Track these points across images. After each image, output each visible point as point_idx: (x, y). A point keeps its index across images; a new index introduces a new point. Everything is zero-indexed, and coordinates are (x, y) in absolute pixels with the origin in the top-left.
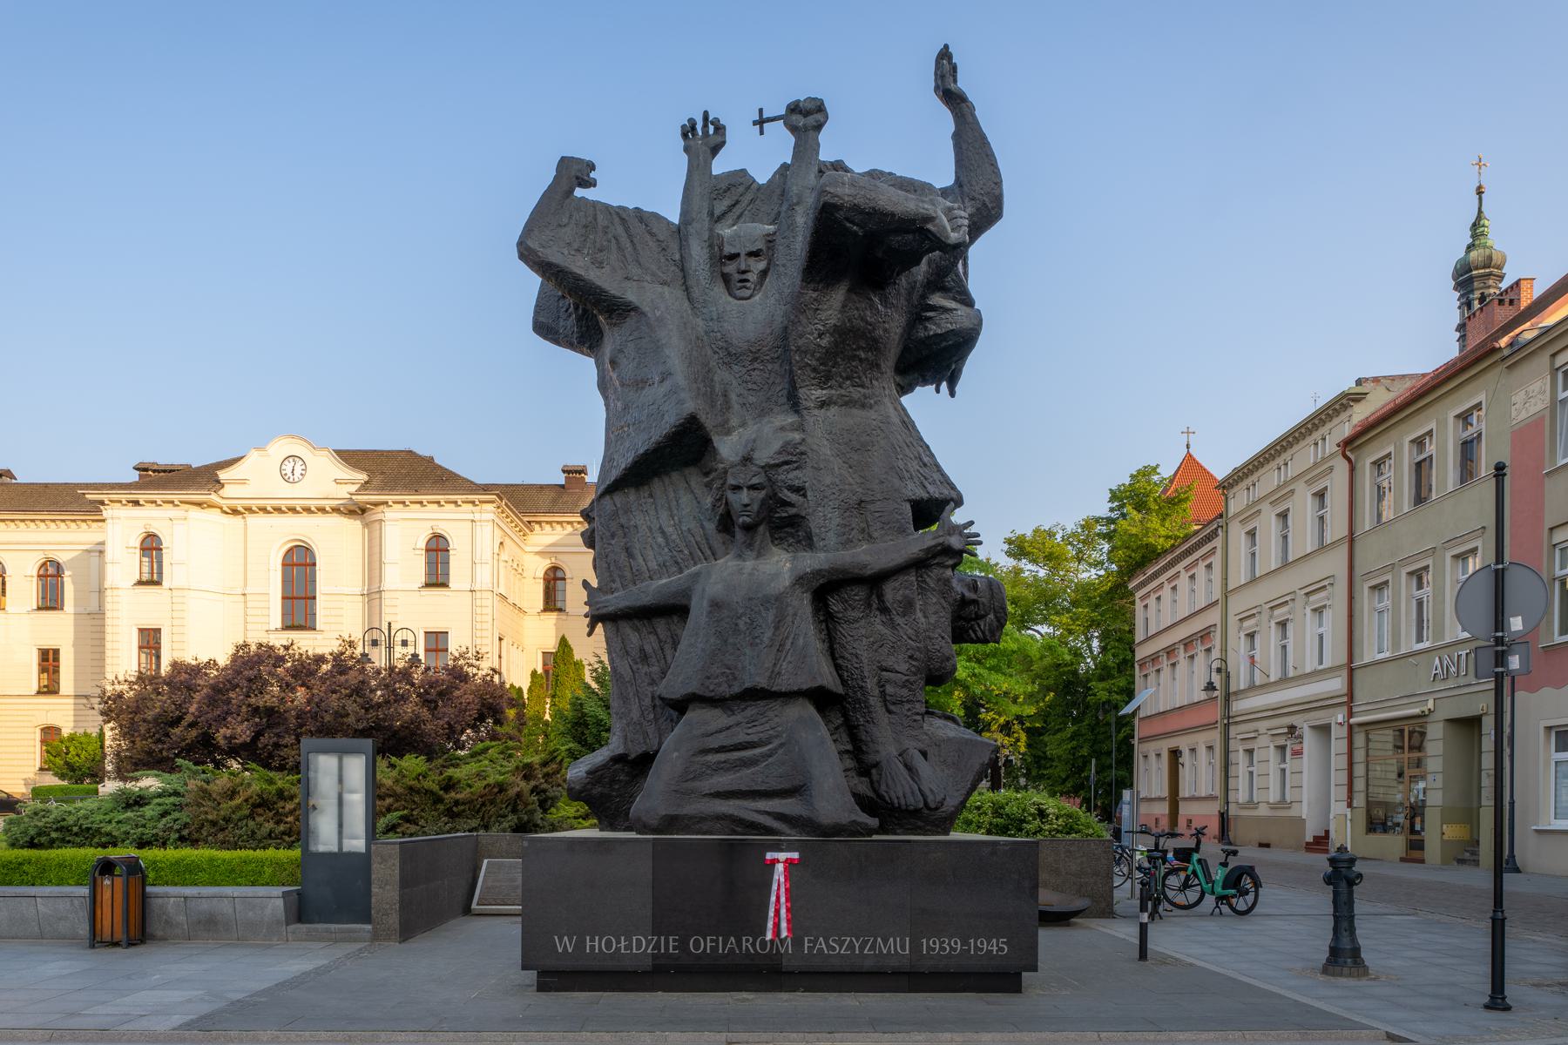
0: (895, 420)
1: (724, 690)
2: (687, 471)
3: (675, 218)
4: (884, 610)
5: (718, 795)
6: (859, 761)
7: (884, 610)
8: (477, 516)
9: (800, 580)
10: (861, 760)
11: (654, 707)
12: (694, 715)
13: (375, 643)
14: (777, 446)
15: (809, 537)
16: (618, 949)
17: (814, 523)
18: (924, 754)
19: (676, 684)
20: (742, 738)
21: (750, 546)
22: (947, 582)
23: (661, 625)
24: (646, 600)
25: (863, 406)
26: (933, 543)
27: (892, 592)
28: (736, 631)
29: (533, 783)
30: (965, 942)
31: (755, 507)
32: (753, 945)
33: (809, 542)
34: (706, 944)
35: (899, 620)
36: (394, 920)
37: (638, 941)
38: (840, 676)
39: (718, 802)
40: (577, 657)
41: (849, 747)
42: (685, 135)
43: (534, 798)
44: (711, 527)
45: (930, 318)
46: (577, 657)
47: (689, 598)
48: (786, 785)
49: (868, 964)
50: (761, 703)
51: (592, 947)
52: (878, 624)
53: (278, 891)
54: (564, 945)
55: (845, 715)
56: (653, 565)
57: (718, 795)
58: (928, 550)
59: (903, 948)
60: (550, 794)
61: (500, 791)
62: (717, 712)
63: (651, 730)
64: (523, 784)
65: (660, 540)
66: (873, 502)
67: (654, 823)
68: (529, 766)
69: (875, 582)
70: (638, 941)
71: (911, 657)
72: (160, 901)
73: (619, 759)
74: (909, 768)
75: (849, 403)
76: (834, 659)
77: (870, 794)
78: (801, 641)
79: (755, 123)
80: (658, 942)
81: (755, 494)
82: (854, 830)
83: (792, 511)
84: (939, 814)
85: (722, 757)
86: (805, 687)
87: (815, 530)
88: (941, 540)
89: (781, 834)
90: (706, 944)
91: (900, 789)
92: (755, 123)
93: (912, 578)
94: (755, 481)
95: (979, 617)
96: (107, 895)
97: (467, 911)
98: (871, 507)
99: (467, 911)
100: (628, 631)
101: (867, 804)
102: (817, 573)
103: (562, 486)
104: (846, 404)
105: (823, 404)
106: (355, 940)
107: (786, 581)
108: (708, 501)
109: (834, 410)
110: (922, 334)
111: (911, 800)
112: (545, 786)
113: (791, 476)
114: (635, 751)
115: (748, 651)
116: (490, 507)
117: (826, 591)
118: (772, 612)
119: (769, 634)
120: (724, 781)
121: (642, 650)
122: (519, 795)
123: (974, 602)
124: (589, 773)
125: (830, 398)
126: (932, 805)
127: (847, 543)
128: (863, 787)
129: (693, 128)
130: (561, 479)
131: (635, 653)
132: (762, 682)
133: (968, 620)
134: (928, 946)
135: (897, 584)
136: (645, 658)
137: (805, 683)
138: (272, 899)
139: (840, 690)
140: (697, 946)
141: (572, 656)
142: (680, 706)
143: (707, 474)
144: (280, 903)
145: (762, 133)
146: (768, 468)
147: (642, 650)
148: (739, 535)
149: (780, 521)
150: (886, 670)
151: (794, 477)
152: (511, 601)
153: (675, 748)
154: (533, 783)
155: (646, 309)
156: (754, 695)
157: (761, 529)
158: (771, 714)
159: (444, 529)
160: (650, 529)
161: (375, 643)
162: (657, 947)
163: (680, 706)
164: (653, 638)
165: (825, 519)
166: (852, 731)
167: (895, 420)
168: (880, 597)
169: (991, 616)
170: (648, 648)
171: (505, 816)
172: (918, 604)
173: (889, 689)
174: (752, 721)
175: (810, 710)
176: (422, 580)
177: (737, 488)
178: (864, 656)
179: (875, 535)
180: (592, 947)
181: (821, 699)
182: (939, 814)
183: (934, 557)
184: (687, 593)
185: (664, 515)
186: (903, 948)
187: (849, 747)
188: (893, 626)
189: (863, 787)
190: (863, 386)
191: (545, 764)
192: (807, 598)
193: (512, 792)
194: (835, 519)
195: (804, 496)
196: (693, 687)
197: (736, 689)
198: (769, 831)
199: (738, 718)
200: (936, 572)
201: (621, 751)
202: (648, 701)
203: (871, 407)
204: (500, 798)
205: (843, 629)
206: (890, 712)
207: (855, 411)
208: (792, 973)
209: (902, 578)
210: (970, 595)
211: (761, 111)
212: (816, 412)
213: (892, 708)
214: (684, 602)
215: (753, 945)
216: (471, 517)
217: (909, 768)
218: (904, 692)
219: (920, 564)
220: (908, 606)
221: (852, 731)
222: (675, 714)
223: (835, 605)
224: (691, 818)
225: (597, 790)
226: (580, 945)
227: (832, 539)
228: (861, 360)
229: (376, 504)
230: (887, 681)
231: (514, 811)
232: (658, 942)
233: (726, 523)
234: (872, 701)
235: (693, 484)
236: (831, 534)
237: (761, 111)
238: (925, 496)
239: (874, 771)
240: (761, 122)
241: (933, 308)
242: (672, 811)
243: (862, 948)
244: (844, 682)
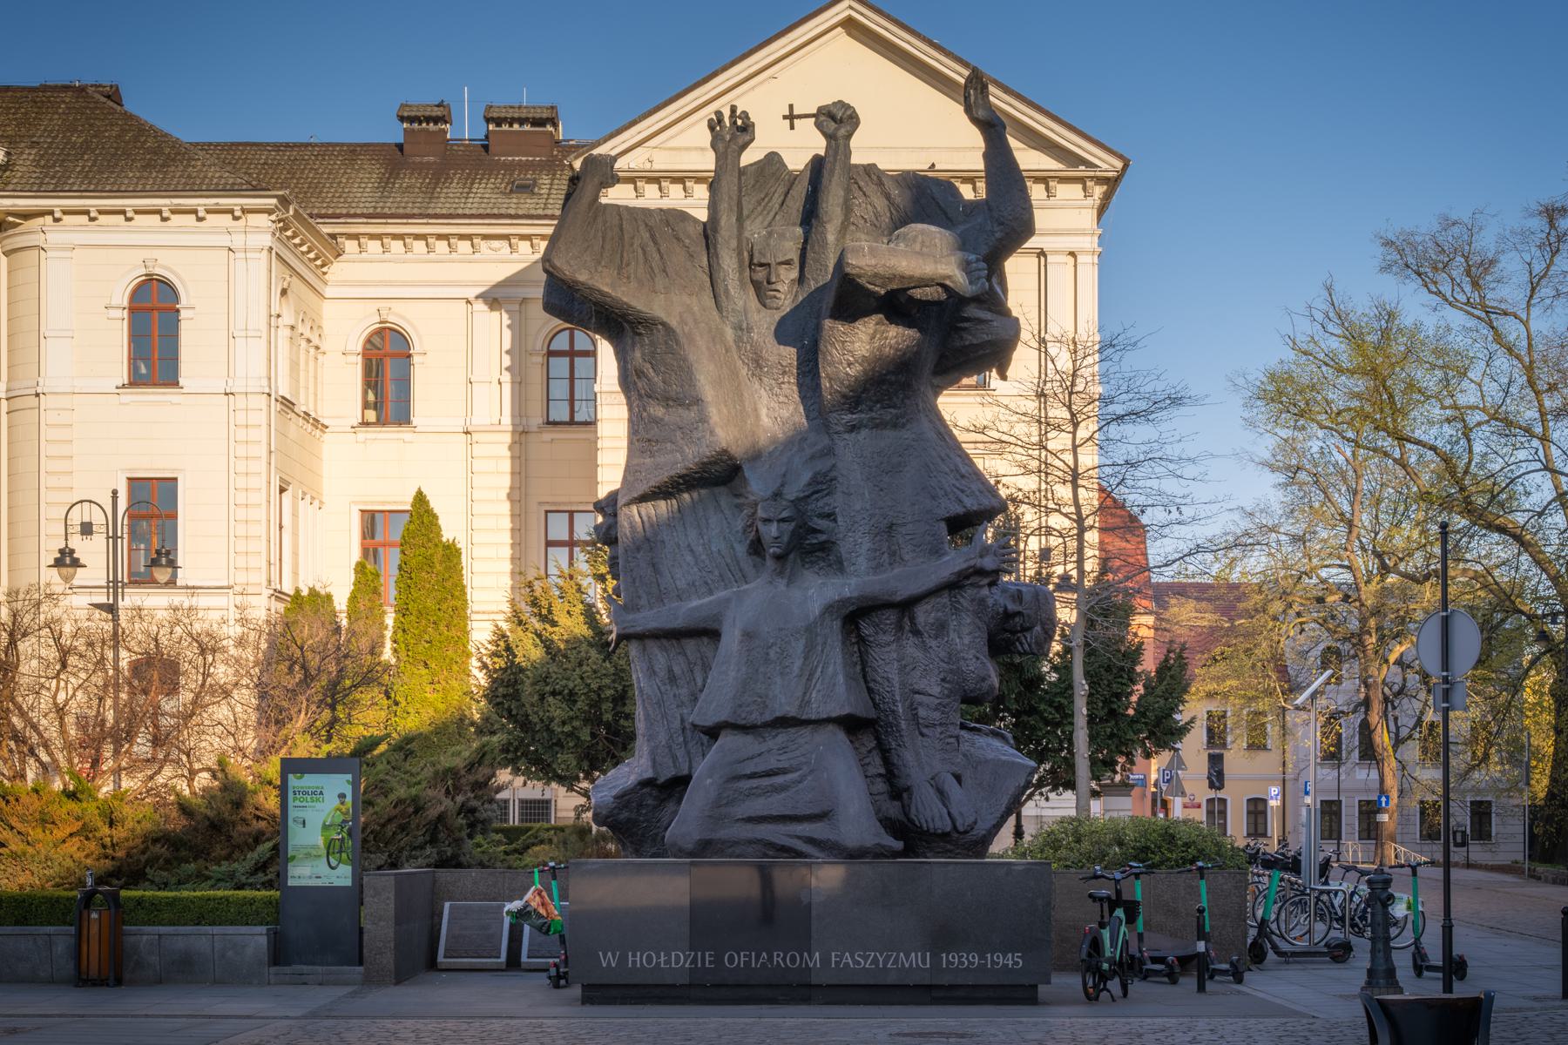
0: (931, 435)
1: (756, 718)
2: (717, 490)
3: (702, 215)
4: (916, 633)
5: (750, 820)
6: (892, 785)
7: (916, 633)
8: (238, 241)
9: (829, 609)
10: (895, 787)
11: (684, 729)
12: (726, 740)
13: (87, 529)
14: (806, 476)
15: (840, 562)
16: (658, 964)
17: (844, 548)
18: (958, 778)
19: (712, 710)
20: (773, 763)
21: (781, 573)
22: (982, 601)
23: (690, 645)
24: (679, 623)
25: (895, 426)
26: (965, 566)
27: (924, 615)
28: (767, 660)
29: (460, 799)
30: (983, 957)
31: (786, 539)
32: (784, 959)
33: (839, 566)
34: (740, 959)
35: (933, 643)
36: (388, 960)
37: (677, 957)
38: (873, 699)
39: (749, 826)
40: (447, 536)
41: (882, 771)
42: (712, 128)
43: (461, 821)
44: (741, 550)
45: (965, 329)
46: (447, 536)
47: (720, 622)
48: (816, 811)
49: (891, 979)
50: (792, 730)
51: (634, 962)
52: (910, 647)
53: (263, 929)
54: (608, 960)
55: (878, 738)
56: (681, 584)
57: (750, 820)
58: (960, 573)
59: (924, 962)
60: (482, 815)
61: (416, 812)
62: (749, 739)
63: (680, 753)
64: (447, 802)
65: (689, 558)
66: (904, 525)
67: (690, 846)
68: (453, 772)
69: (906, 606)
70: (677, 957)
71: (943, 680)
72: (132, 939)
73: (648, 783)
74: (941, 792)
75: (879, 425)
76: (866, 682)
77: (902, 818)
78: (831, 669)
79: (785, 117)
80: (695, 957)
81: (785, 526)
82: (879, 853)
83: (823, 538)
84: (968, 837)
85: (755, 782)
86: (834, 715)
87: (845, 556)
88: (972, 563)
89: (810, 856)
90: (740, 959)
91: (929, 812)
92: (785, 117)
93: (944, 599)
94: (785, 514)
95: (1025, 630)
96: (94, 929)
97: (432, 965)
98: (903, 530)
99: (432, 965)
100: (656, 651)
101: (894, 827)
102: (844, 602)
103: (400, 147)
104: (876, 426)
105: (853, 428)
106: (346, 984)
107: (815, 608)
108: (739, 524)
109: (864, 433)
110: (958, 344)
111: (938, 824)
112: (474, 803)
113: (820, 504)
114: (666, 774)
115: (778, 680)
116: (263, 220)
117: (855, 617)
118: (803, 641)
119: (798, 663)
120: (758, 806)
121: (670, 670)
122: (441, 818)
123: (1019, 613)
124: (616, 797)
125: (861, 421)
126: (961, 829)
127: (877, 568)
128: (893, 809)
129: (720, 121)
130: (394, 133)
131: (662, 674)
132: (791, 710)
133: (1014, 632)
134: (948, 962)
135: (929, 607)
136: (673, 679)
137: (837, 711)
138: (256, 938)
139: (872, 714)
140: (731, 959)
141: (439, 535)
142: (713, 733)
143: (737, 496)
144: (263, 940)
145: (792, 127)
146: (795, 503)
147: (670, 670)
148: (770, 563)
149: (807, 545)
150: (918, 693)
151: (821, 504)
152: (300, 408)
153: (707, 771)
154: (460, 799)
155: (674, 323)
156: (784, 722)
157: (791, 556)
158: (801, 741)
159: (169, 266)
160: (678, 546)
161: (87, 529)
162: (694, 961)
163: (713, 733)
164: (681, 659)
165: (856, 544)
166: (885, 752)
167: (931, 435)
168: (912, 619)
169: (1038, 628)
170: (677, 670)
171: (422, 847)
172: (953, 624)
173: (922, 712)
174: (783, 749)
175: (841, 736)
176: (124, 378)
177: (767, 521)
178: (896, 679)
179: (907, 557)
180: (634, 962)
181: (852, 725)
182: (968, 837)
183: (967, 577)
184: (718, 618)
185: (693, 534)
186: (924, 962)
187: (882, 771)
188: (926, 648)
189: (893, 809)
190: (894, 407)
191: (471, 767)
192: (837, 625)
193: (433, 813)
194: (866, 544)
195: (835, 520)
196: (723, 716)
197: (768, 717)
198: (800, 854)
199: (771, 744)
200: (970, 592)
201: (649, 774)
202: (677, 724)
203: (904, 426)
204: (415, 821)
205: (875, 653)
206: (922, 735)
207: (887, 433)
208: (820, 986)
209: (933, 601)
210: (1012, 607)
211: (791, 107)
212: (846, 436)
213: (925, 731)
214: (715, 626)
215: (784, 959)
216: (225, 240)
217: (941, 792)
218: (937, 715)
219: (954, 585)
220: (941, 628)
221: (885, 752)
222: (705, 738)
223: (867, 629)
224: (724, 842)
225: (625, 815)
226: (623, 958)
227: (862, 563)
228: (891, 384)
229: (27, 216)
230: (920, 704)
231: (433, 841)
232: (695, 957)
233: (757, 548)
234: (903, 725)
235: (723, 503)
236: (861, 559)
237: (791, 107)
238: (960, 510)
239: (905, 795)
240: (791, 117)
241: (968, 320)
242: (708, 836)
243: (886, 962)
244: (876, 706)
